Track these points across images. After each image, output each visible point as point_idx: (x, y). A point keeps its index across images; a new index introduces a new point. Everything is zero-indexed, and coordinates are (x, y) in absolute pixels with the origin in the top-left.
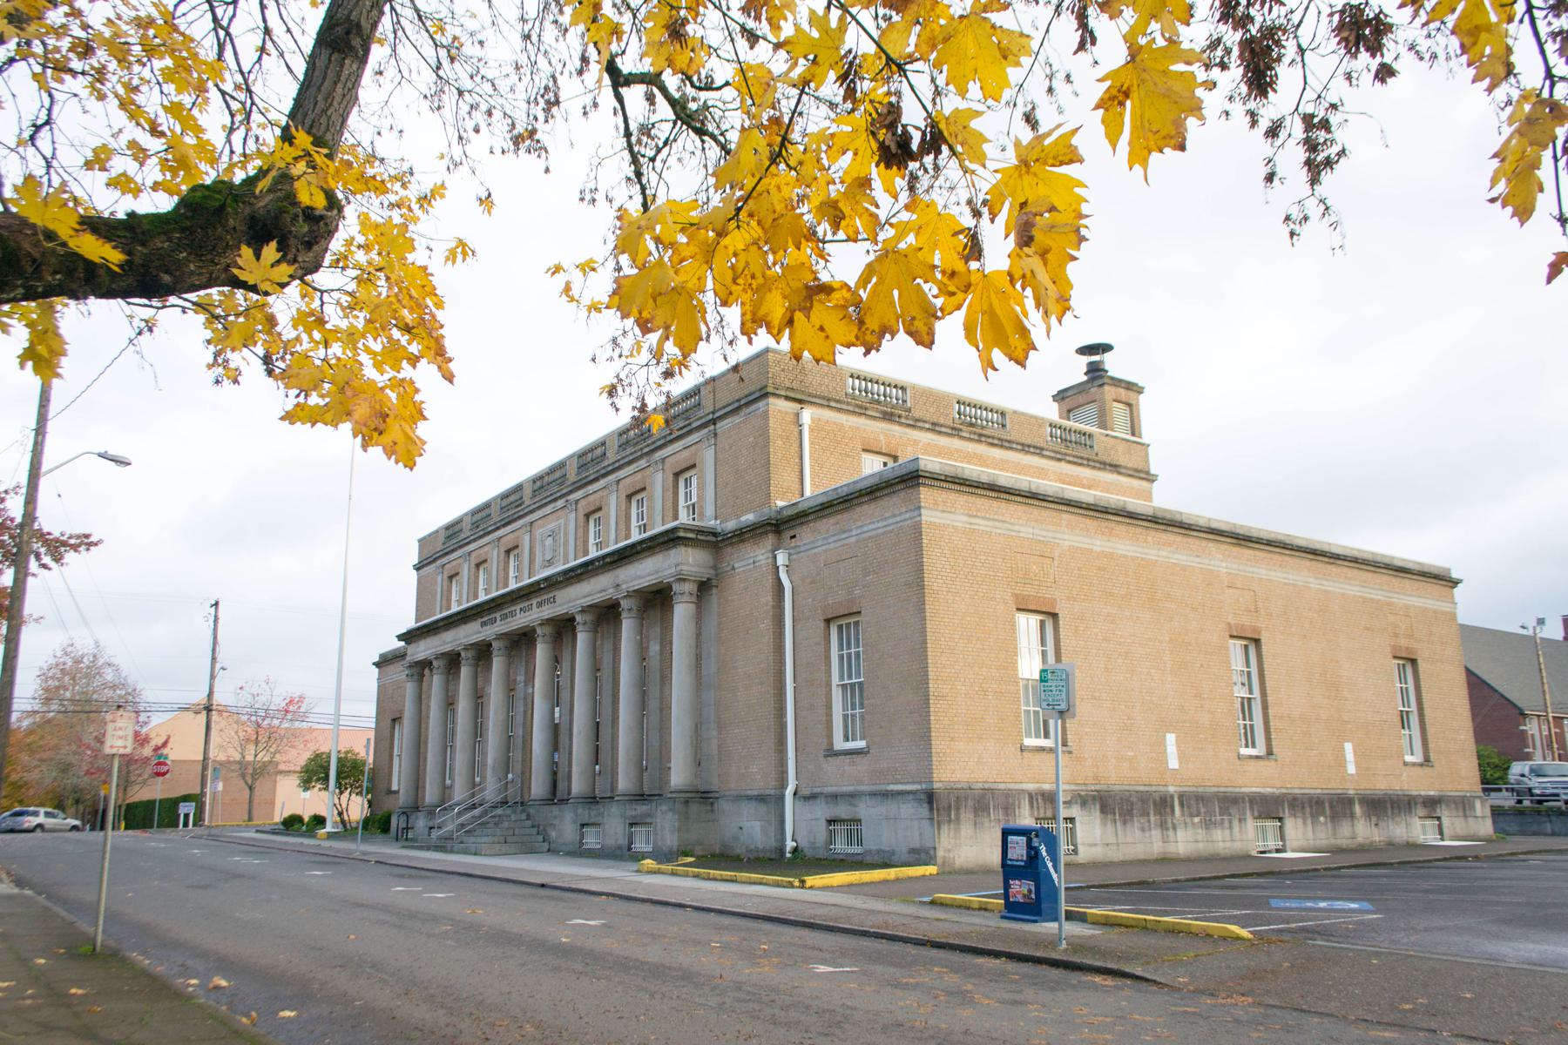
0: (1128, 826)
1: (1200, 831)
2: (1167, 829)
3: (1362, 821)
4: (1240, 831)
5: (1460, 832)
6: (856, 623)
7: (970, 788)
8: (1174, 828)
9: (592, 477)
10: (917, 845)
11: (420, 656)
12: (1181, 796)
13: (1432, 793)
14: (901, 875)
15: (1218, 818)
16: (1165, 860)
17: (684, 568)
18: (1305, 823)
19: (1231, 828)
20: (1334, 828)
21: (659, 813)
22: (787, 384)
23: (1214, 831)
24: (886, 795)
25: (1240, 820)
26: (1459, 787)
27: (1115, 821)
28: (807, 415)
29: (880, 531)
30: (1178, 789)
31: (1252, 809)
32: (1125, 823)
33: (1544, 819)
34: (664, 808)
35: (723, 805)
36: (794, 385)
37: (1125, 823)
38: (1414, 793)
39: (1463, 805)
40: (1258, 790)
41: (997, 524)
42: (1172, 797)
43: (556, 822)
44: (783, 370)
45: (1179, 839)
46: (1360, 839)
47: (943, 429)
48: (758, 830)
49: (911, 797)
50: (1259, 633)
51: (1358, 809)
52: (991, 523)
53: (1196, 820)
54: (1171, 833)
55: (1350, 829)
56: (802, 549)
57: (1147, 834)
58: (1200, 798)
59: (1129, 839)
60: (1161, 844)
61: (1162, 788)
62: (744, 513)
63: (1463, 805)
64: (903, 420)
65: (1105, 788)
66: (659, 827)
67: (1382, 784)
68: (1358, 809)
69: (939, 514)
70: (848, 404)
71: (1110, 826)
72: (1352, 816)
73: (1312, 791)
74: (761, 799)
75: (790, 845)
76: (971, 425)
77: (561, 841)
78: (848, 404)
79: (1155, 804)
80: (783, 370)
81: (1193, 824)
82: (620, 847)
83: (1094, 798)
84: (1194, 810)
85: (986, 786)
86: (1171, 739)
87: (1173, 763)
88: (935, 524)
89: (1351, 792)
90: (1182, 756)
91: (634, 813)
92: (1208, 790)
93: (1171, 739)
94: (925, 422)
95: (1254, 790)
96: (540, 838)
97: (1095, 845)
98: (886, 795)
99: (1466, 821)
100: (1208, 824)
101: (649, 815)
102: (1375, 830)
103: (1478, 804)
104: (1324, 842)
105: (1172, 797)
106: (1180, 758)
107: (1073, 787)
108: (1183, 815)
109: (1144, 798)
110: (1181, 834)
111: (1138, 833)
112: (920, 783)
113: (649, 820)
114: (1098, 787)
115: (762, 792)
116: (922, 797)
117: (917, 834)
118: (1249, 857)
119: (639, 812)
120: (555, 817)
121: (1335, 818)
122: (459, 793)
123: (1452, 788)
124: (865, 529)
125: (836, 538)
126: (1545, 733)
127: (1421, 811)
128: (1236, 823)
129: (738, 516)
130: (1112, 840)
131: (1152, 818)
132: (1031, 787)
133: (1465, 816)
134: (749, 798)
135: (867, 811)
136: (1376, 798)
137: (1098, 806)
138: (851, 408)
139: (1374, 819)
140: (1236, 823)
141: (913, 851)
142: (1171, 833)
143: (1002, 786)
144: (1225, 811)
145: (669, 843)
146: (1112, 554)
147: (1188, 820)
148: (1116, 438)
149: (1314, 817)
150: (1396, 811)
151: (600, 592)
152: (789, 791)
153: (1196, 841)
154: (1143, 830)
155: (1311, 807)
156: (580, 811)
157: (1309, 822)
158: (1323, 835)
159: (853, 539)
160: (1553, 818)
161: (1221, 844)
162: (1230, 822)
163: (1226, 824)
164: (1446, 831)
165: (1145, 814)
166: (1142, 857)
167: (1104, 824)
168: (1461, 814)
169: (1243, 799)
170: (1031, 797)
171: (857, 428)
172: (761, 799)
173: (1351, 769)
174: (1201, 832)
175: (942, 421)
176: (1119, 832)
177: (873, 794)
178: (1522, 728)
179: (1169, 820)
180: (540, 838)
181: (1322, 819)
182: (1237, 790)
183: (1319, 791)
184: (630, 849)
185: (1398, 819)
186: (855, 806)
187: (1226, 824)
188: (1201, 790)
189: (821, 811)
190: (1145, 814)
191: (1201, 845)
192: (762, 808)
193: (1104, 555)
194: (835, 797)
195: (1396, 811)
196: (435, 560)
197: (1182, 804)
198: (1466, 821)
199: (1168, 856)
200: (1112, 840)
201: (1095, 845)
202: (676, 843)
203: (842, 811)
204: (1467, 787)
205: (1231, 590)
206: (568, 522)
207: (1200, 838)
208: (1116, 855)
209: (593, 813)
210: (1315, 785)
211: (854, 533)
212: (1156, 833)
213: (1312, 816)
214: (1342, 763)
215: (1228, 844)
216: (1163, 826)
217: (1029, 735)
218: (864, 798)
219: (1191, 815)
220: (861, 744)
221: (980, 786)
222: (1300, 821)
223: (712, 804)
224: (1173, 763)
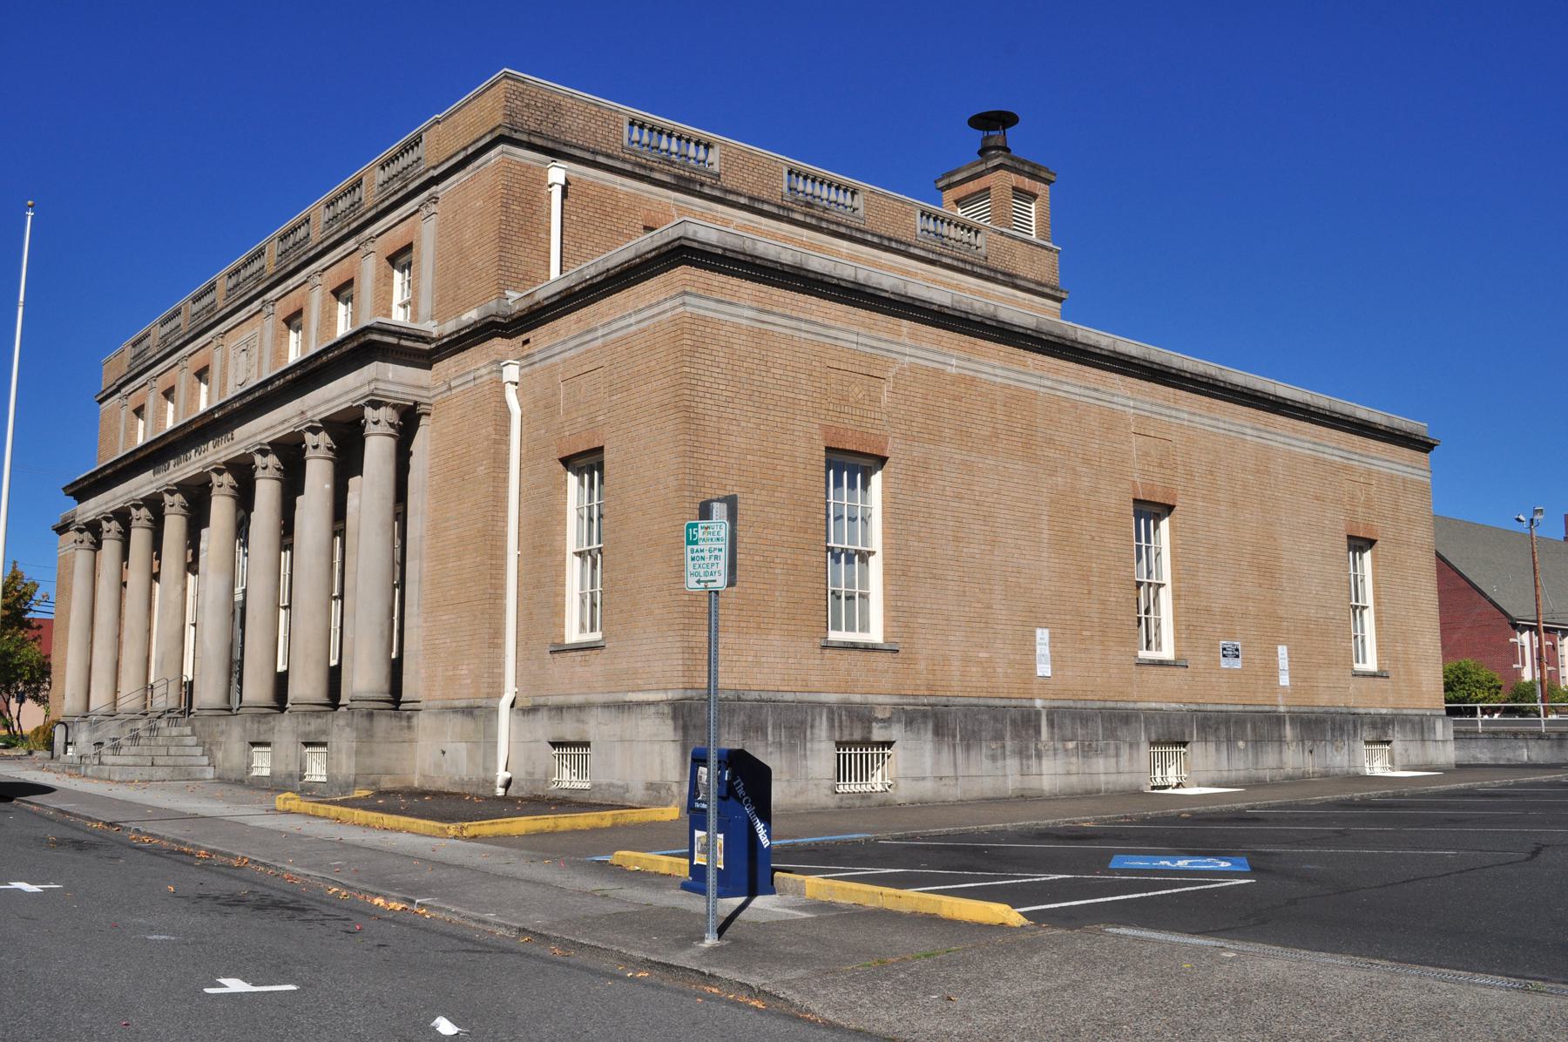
0: (973, 753)
1: (1074, 760)
2: (1029, 757)
3: (1293, 747)
4: (1131, 759)
5: (1414, 760)
6: (408, 420)
7: (739, 699)
8: (1039, 756)
9: (291, 267)
10: (656, 779)
11: (90, 517)
12: (1051, 712)
13: (1384, 711)
14: (621, 820)
15: (1102, 744)
16: (1024, 798)
17: (381, 385)
18: (1218, 750)
19: (1117, 755)
20: (1256, 756)
21: (335, 730)
22: (533, 126)
23: (1094, 760)
24: (623, 707)
25: (1131, 746)
26: (1418, 704)
27: (954, 746)
28: (557, 173)
29: (634, 328)
30: (1048, 704)
31: (1147, 730)
32: (968, 748)
33: (1521, 744)
34: (342, 722)
35: (421, 721)
36: (543, 129)
37: (968, 748)
38: (1362, 711)
39: (1419, 726)
40: (1158, 706)
41: (804, 326)
42: (1038, 713)
43: (222, 739)
44: (528, 106)
45: (1045, 771)
46: (1289, 770)
47: (766, 207)
48: (464, 754)
49: (652, 709)
50: (1175, 500)
51: (1288, 731)
52: (793, 323)
53: (1071, 745)
54: (1034, 761)
55: (1277, 756)
56: (536, 358)
57: (1000, 763)
58: (1082, 717)
59: (973, 771)
60: (1019, 778)
61: (1025, 703)
62: (466, 308)
63: (1419, 726)
64: (707, 190)
65: (943, 700)
66: (334, 749)
67: (1323, 699)
68: (1288, 731)
69: (713, 305)
70: (624, 161)
71: (946, 755)
72: (1281, 740)
73: (1231, 708)
74: (469, 711)
75: (502, 775)
76: (809, 205)
77: (227, 765)
78: (624, 161)
79: (1014, 722)
80: (528, 106)
81: (1066, 750)
82: (290, 775)
83: (925, 715)
84: (1068, 733)
85: (765, 696)
86: (1042, 635)
87: (1044, 669)
88: (704, 318)
89: (1282, 709)
90: (1056, 660)
91: (308, 729)
92: (1089, 705)
93: (1042, 635)
94: (740, 195)
95: (1153, 705)
96: (205, 760)
97: (924, 778)
98: (623, 707)
99: (1423, 745)
100: (1087, 750)
101: (324, 732)
102: (1309, 759)
103: (1439, 725)
104: (1242, 774)
105: (1038, 713)
106: (1053, 661)
107: (896, 700)
108: (1052, 739)
109: (996, 713)
110: (1048, 765)
111: (987, 764)
112: (666, 690)
113: (323, 739)
114: (932, 700)
115: (472, 702)
116: (667, 710)
117: (657, 762)
118: (1139, 793)
119: (312, 728)
120: (222, 733)
121: (1258, 742)
122: (99, 700)
123: (1410, 706)
124: (614, 326)
125: (578, 341)
126: (1536, 646)
127: (1368, 734)
128: (1125, 751)
129: (459, 314)
130: (947, 771)
131: (1009, 744)
132: (832, 698)
133: (1423, 740)
134: (455, 710)
135: (595, 728)
136: (1313, 717)
137: (930, 726)
138: (628, 167)
139: (1308, 744)
140: (1125, 751)
141: (650, 786)
142: (1034, 761)
143: (789, 697)
144: (1111, 734)
145: (344, 771)
146: (973, 379)
147: (1059, 745)
148: (1014, 238)
149: (1231, 741)
150: (1337, 733)
151: (283, 422)
152: (505, 703)
153: (1068, 773)
154: (994, 758)
155: (1228, 729)
156: (248, 725)
157: (1224, 747)
158: (1241, 765)
159: (599, 342)
160: (1532, 743)
161: (1103, 778)
162: (1117, 748)
163: (1112, 751)
164: (1397, 758)
165: (999, 737)
166: (990, 794)
167: (938, 751)
168: (1418, 736)
169: (1137, 716)
170: (831, 710)
171: (636, 196)
172: (469, 711)
173: (1284, 680)
174: (1075, 763)
175: (765, 195)
176: (959, 762)
177: (606, 706)
178: (1512, 640)
179: (1033, 746)
180: (205, 760)
181: (1241, 744)
182: (1131, 705)
183: (1240, 708)
184: (302, 777)
185: (1339, 744)
186: (583, 722)
187: (1112, 751)
188: (1080, 705)
189: (545, 728)
190: (999, 737)
191: (1074, 779)
192: (469, 724)
193: (958, 380)
194: (560, 709)
195: (1337, 733)
196: (118, 390)
197: (1051, 724)
198: (1423, 745)
199: (1029, 793)
200: (947, 771)
201: (924, 778)
202: (353, 771)
203: (569, 731)
204: (1426, 704)
205: (1141, 439)
206: (267, 326)
207: (1074, 769)
208: (953, 792)
209: (263, 727)
210: (1236, 700)
211: (600, 333)
212: (1012, 764)
213: (1229, 740)
214: (1273, 673)
215: (1113, 778)
216: (1022, 754)
217: (837, 627)
218: (595, 711)
219: (1064, 740)
220: (597, 636)
221: (755, 695)
222: (1212, 747)
223: (409, 718)
224: (1044, 669)
